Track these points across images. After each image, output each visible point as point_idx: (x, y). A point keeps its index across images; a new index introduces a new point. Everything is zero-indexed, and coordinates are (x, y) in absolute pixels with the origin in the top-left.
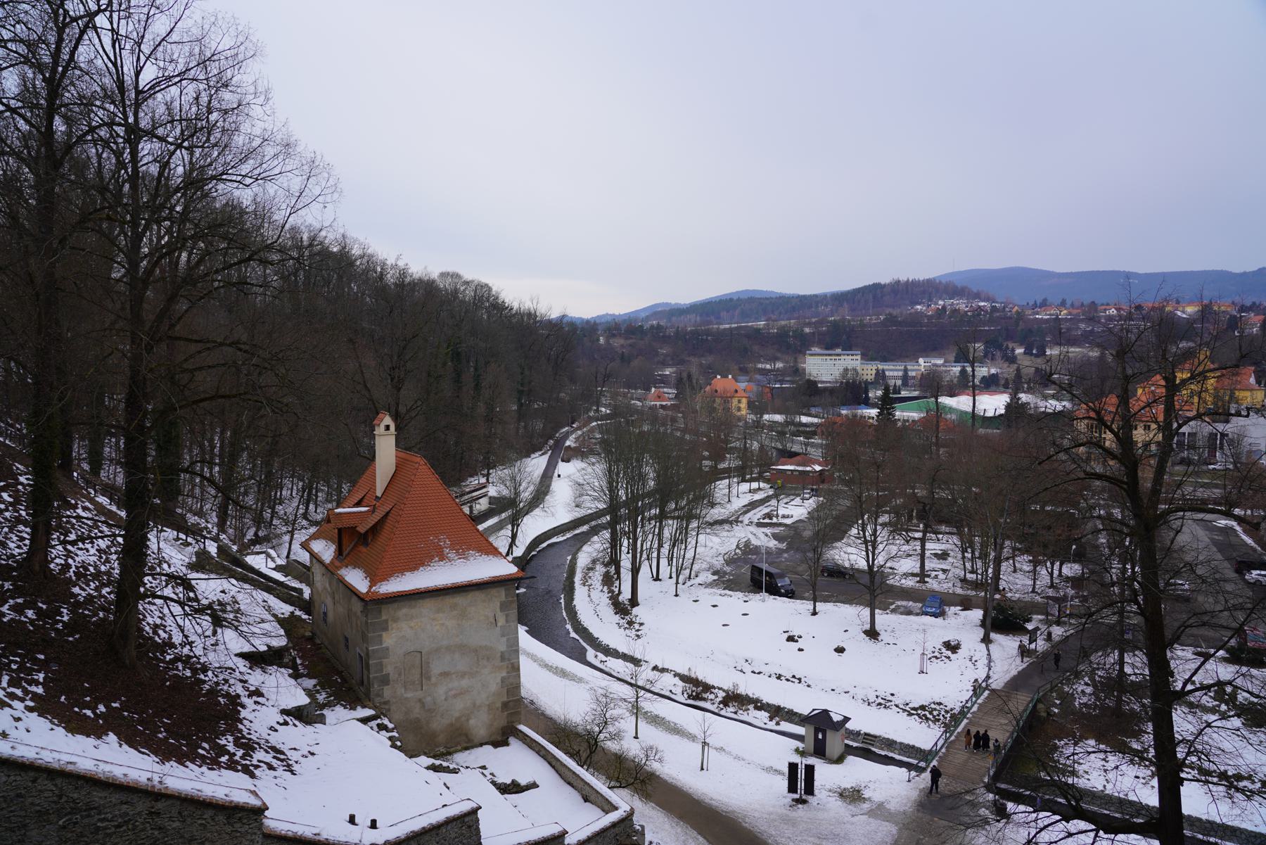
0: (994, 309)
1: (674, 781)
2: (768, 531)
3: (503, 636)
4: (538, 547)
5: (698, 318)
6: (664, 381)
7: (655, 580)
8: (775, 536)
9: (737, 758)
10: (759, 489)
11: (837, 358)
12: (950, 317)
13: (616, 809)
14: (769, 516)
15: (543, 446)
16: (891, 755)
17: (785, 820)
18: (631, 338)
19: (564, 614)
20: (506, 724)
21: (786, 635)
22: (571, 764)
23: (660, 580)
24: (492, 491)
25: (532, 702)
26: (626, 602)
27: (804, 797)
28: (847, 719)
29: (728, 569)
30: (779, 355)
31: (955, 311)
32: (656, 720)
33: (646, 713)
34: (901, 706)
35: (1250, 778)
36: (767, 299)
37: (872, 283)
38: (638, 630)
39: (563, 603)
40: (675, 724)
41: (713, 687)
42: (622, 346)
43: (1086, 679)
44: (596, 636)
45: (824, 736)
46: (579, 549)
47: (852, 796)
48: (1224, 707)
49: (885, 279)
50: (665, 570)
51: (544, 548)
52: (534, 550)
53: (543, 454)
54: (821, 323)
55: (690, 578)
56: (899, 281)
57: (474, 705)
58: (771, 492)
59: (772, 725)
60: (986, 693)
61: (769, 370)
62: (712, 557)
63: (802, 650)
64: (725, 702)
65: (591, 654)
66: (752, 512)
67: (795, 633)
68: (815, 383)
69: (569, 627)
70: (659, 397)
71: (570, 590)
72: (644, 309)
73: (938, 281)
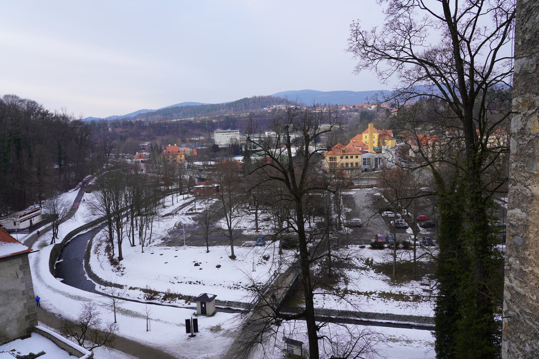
0: (296, 109)
1: (132, 339)
2: (190, 216)
3: (23, 282)
4: (71, 238)
5: (162, 117)
6: (144, 148)
7: (132, 246)
8: (194, 219)
9: (166, 322)
10: (188, 198)
11: (229, 133)
12: (278, 113)
13: (84, 355)
14: (191, 209)
15: (76, 186)
16: (239, 309)
17: (184, 346)
18: (126, 128)
19: (84, 269)
20: (29, 327)
21: (194, 263)
22: (63, 339)
23: (135, 246)
24: (43, 211)
25: (60, 315)
26: (117, 259)
27: (194, 334)
28: (215, 296)
29: (169, 236)
30: (201, 133)
31: (280, 110)
32: (127, 312)
33: (122, 310)
34: (244, 287)
35: (375, 293)
36: (195, 106)
37: (60, 113)
38: (122, 271)
39: (84, 264)
40: (137, 312)
41: (159, 292)
42: (121, 132)
43: (319, 264)
44: (100, 277)
45: (205, 306)
46: (93, 237)
47: (216, 329)
48: (368, 267)
49: (249, 96)
50: (137, 241)
51: (75, 238)
52: (69, 240)
53: (76, 190)
54: (221, 117)
55: (150, 243)
56: (256, 97)
57: (8, 320)
58: (193, 199)
59: (187, 305)
60: (279, 275)
61: (197, 141)
62: (162, 232)
63: (201, 269)
64: (164, 299)
65: (98, 287)
66: (184, 208)
67: (198, 262)
68: (217, 146)
69: (86, 275)
70: (140, 157)
71: (87, 257)
72: (134, 113)
73: (273, 96)
